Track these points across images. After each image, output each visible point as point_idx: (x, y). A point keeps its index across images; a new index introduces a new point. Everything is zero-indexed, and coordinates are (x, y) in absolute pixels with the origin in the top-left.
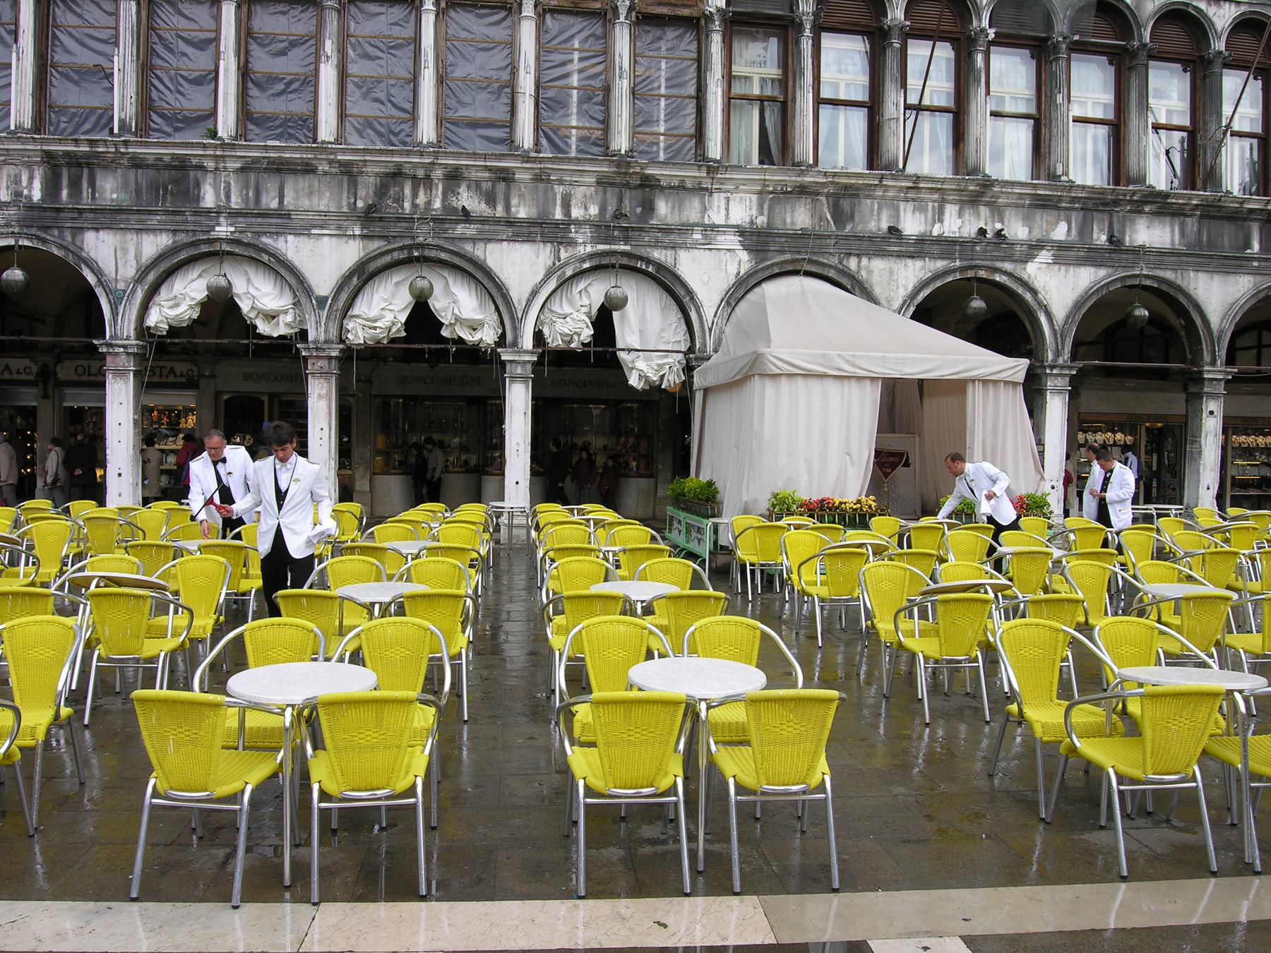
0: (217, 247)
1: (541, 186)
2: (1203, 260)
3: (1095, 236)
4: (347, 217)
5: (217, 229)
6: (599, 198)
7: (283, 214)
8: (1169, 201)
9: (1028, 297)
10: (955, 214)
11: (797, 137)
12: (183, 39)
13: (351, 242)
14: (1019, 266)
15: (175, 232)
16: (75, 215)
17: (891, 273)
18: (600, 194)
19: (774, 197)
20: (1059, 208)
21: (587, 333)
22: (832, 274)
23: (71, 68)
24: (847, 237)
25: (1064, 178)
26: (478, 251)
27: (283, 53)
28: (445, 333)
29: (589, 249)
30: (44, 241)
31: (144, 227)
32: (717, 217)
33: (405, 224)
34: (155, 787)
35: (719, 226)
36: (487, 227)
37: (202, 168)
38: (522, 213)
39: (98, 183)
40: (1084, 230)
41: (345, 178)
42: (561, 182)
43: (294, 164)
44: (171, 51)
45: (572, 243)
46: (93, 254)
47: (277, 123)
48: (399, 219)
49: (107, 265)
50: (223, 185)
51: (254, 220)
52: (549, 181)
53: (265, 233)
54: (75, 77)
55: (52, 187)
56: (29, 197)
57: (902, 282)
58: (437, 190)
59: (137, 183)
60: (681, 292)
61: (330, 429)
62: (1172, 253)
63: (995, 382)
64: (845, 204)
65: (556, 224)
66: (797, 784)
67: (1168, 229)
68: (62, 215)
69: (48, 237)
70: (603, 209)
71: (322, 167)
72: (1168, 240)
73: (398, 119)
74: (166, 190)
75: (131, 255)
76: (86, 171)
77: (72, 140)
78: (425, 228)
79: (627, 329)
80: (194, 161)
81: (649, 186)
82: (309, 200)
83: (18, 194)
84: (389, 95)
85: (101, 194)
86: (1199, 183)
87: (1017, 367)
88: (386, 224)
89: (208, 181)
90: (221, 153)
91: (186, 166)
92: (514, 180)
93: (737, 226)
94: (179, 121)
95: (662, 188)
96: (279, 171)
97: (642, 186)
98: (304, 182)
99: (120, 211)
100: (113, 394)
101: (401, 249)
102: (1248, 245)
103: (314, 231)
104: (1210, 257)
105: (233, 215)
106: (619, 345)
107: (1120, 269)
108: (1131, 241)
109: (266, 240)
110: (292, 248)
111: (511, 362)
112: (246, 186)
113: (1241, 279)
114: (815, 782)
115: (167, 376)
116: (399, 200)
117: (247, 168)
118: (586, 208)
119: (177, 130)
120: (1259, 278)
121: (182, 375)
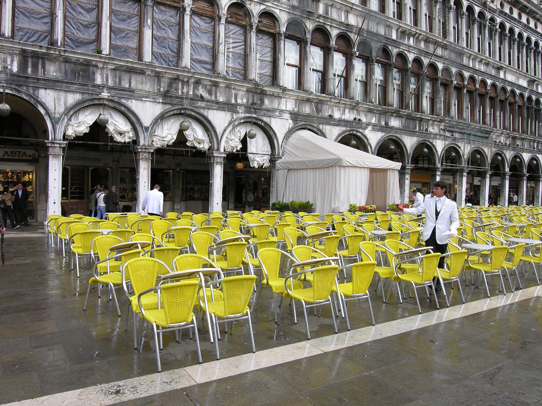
0: (102, 102)
1: (227, 89)
4: (157, 95)
5: (102, 94)
6: (246, 96)
7: (131, 91)
9: (366, 141)
10: (348, 112)
11: (305, 81)
12: (81, 6)
13: (158, 105)
14: (364, 131)
15: (83, 93)
16: (35, 81)
17: (331, 131)
18: (247, 95)
19: (300, 102)
20: (373, 113)
21: (240, 146)
22: (315, 130)
23: (25, 10)
24: (320, 118)
25: (375, 103)
26: (205, 113)
27: (124, 20)
28: (188, 144)
29: (243, 115)
30: (19, 91)
31: (69, 90)
32: (283, 107)
33: (179, 100)
35: (284, 110)
36: (209, 104)
37: (96, 66)
38: (221, 99)
39: (47, 67)
40: (379, 121)
41: (156, 78)
42: (234, 89)
43: (137, 70)
44: (74, 10)
45: (237, 112)
46: (43, 100)
47: (122, 50)
48: (177, 97)
49: (50, 105)
50: (105, 75)
51: (118, 92)
52: (230, 88)
53: (123, 98)
54: (28, 15)
55: (23, 66)
56: (11, 70)
57: (334, 134)
58: (191, 87)
59: (65, 69)
60: (272, 133)
61: (148, 182)
62: (400, 129)
63: (394, 170)
64: (319, 106)
65: (233, 105)
66: (183, 322)
68: (29, 80)
69: (22, 90)
70: (248, 101)
71: (149, 72)
73: (172, 56)
74: (79, 74)
75: (62, 102)
76: (40, 61)
77: (39, 46)
78: (187, 102)
79: (252, 146)
80: (94, 63)
81: (263, 93)
82: (142, 86)
83: (5, 68)
84: (169, 45)
85: (48, 72)
86: (404, 108)
87: (398, 165)
88: (172, 99)
89: (99, 72)
90: (108, 61)
91: (89, 65)
92: (218, 86)
93: (289, 111)
94: (78, 43)
95: (266, 95)
96: (129, 72)
97: (260, 93)
98: (139, 78)
99: (58, 81)
100: (52, 166)
101: (177, 109)
102: (416, 128)
103: (143, 99)
104: (408, 131)
105: (110, 88)
106: (249, 151)
109: (123, 101)
110: (134, 105)
111: (217, 156)
112: (115, 77)
114: (190, 320)
115: (22, 156)
116: (177, 89)
117: (116, 69)
118: (242, 100)
119: (77, 47)
121: (30, 156)
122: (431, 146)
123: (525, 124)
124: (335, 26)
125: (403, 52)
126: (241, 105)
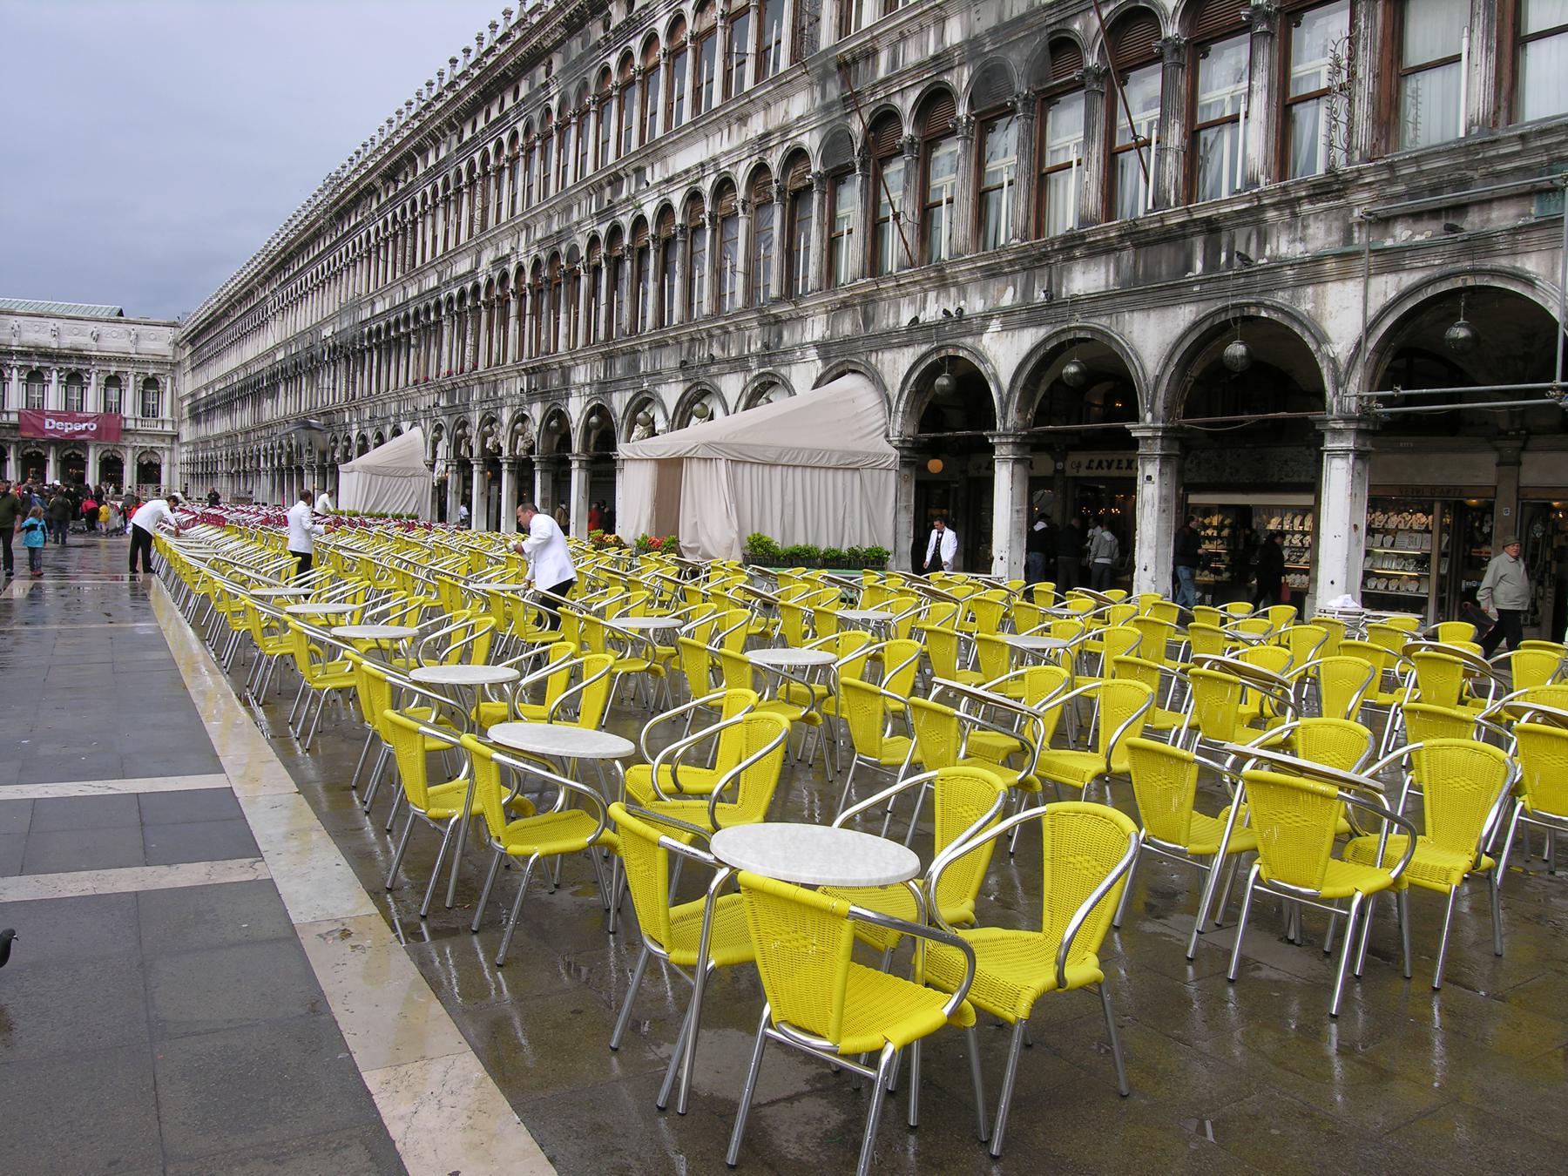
2: (1136, 297)
3: (1036, 294)
8: (1087, 240)
10: (934, 299)
34: (1258, 874)
57: (901, 369)
67: (1103, 270)
72: (1103, 282)
102: (1189, 267)
104: (1144, 292)
107: (1058, 325)
108: (1067, 292)
111: (1143, 438)
113: (1181, 312)
120: (1202, 305)
122: (923, 367)
123: (384, 368)
124: (909, 83)
125: (937, 82)
126: (751, 355)
